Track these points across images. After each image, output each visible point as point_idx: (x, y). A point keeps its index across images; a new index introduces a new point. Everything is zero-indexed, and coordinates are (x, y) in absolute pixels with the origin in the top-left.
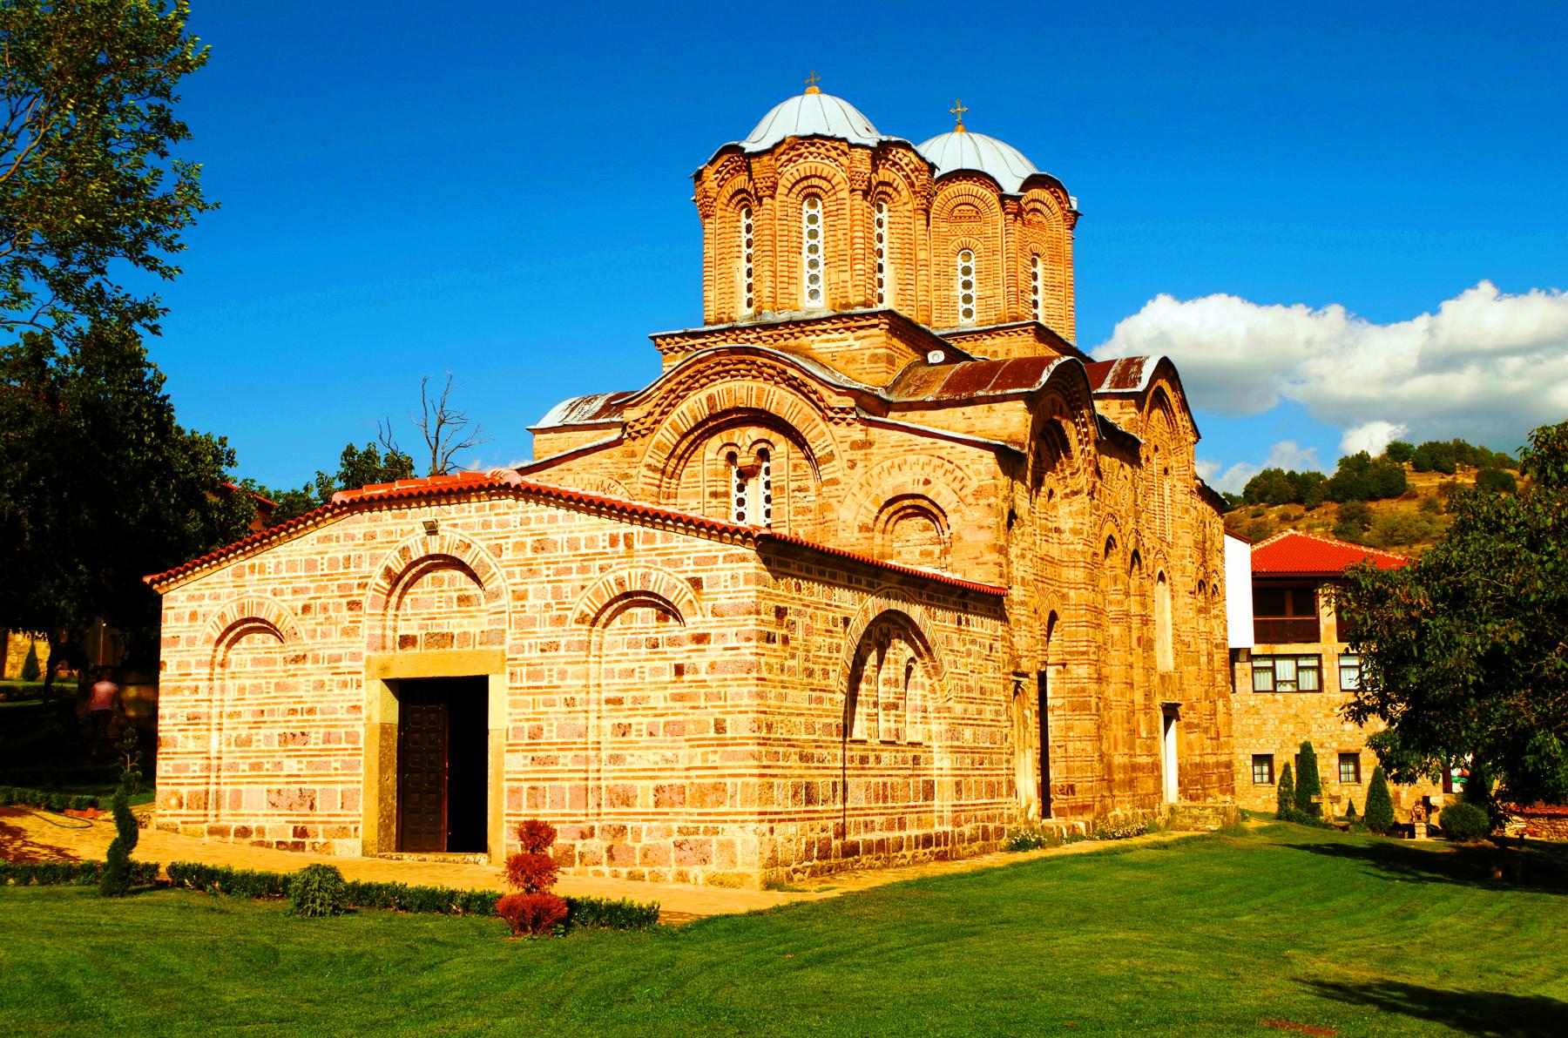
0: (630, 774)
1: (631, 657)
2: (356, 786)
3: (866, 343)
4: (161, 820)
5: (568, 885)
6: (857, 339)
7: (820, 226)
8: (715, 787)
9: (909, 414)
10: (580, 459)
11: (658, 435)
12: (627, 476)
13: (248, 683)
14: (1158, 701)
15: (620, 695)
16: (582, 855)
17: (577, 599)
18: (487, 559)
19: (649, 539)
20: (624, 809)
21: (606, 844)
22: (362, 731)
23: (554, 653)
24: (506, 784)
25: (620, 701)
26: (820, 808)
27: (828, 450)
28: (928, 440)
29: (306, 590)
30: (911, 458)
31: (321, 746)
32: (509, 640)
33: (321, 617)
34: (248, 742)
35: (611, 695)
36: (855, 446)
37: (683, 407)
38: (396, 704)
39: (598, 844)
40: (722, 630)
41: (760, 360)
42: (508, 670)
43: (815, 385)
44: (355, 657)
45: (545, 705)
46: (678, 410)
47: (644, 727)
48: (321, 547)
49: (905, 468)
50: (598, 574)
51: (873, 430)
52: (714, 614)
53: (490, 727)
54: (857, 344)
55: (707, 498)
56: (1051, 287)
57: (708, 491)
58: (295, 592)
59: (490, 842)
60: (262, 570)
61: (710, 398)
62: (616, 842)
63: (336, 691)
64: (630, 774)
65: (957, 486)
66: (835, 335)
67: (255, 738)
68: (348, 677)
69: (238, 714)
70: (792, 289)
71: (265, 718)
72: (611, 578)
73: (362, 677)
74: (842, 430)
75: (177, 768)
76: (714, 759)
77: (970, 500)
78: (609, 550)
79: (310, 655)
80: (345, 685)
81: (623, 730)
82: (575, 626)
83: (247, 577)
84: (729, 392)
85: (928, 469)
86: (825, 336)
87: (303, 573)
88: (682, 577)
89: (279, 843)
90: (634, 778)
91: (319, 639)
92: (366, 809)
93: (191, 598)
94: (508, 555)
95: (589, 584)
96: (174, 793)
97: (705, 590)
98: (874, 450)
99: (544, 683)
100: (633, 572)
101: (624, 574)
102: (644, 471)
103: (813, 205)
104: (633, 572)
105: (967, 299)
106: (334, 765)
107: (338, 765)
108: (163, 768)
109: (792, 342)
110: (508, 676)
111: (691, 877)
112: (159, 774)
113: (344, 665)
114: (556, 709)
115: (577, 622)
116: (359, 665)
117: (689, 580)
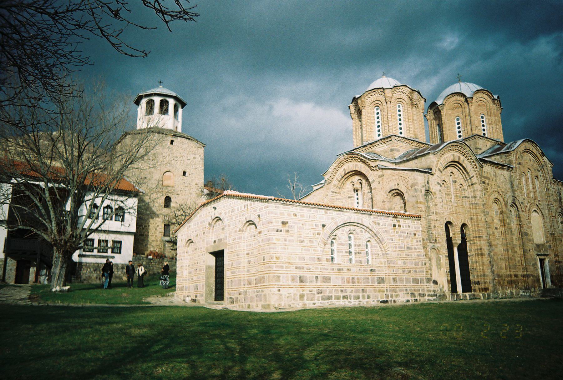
11: (333, 183)
12: (327, 195)
19: (251, 205)
26: (308, 284)
28: (398, 171)
30: (394, 178)
36: (380, 177)
37: (338, 173)
38: (214, 258)
41: (354, 156)
43: (367, 161)
49: (392, 181)
51: (384, 171)
53: (225, 263)
56: (490, 124)
61: (344, 169)
65: (406, 184)
66: (381, 145)
70: (372, 135)
74: (376, 173)
76: (263, 269)
77: (410, 188)
85: (398, 180)
86: (378, 146)
98: (384, 177)
103: (377, 109)
105: (459, 132)
109: (371, 150)
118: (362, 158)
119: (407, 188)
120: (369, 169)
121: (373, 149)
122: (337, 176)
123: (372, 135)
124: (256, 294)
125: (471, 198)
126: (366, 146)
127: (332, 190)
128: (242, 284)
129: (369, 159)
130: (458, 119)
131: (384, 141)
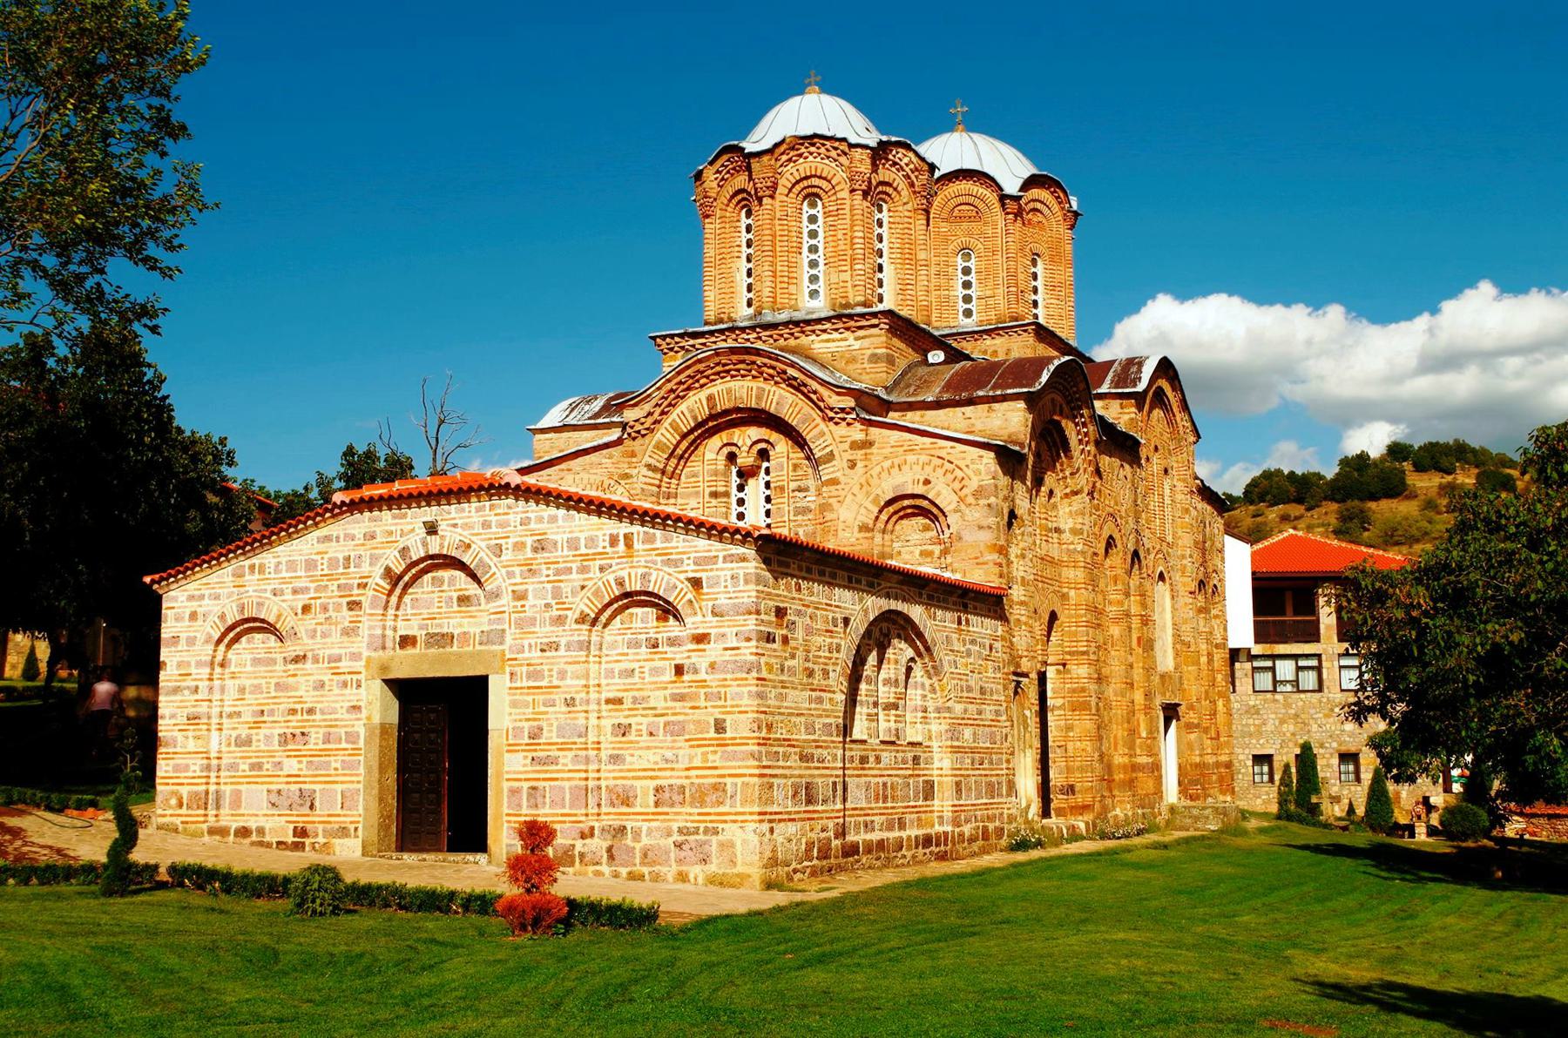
6: (857, 339)
9: (909, 414)
11: (658, 436)
12: (627, 476)
15: (620, 695)
16: (582, 855)
18: (486, 559)
20: (624, 809)
21: (605, 845)
22: (362, 731)
23: (554, 653)
25: (620, 701)
26: (820, 808)
29: (305, 590)
30: (911, 458)
32: (509, 640)
33: (321, 617)
35: (611, 695)
36: (855, 446)
37: (683, 407)
40: (722, 630)
41: (759, 360)
42: (508, 670)
43: (815, 385)
44: (355, 657)
46: (678, 411)
47: (644, 727)
50: (598, 574)
51: (873, 430)
52: (714, 614)
54: (857, 345)
55: (707, 498)
56: (1051, 287)
57: (707, 491)
58: (295, 592)
60: (262, 569)
61: (710, 398)
63: (336, 691)
65: (957, 485)
66: (835, 335)
68: (348, 677)
69: (239, 714)
70: (793, 289)
71: (265, 718)
72: (611, 578)
73: (362, 677)
74: (842, 430)
75: (177, 768)
77: (971, 500)
78: (609, 550)
79: (309, 655)
80: (345, 685)
81: (623, 730)
84: (729, 391)
85: (928, 469)
86: (825, 336)
87: (303, 573)
88: (682, 577)
89: (279, 843)
90: (634, 778)
92: (366, 809)
93: (191, 598)
94: (507, 555)
96: (174, 793)
97: (705, 590)
98: (874, 450)
99: (544, 683)
100: (633, 572)
102: (644, 471)
103: (813, 205)
104: (633, 572)
105: (967, 299)
106: (334, 765)
108: (163, 768)
109: (792, 342)
110: (508, 677)
113: (345, 665)
114: (556, 709)
115: (577, 622)
117: (689, 580)
118: (791, 372)
119: (962, 499)
120: (816, 414)
121: (804, 340)
122: (674, 415)
123: (793, 289)
124: (677, 837)
125: (1067, 536)
126: (774, 326)
127: (647, 460)
128: (592, 801)
129: (824, 383)
130: (967, 257)
131: (840, 325)
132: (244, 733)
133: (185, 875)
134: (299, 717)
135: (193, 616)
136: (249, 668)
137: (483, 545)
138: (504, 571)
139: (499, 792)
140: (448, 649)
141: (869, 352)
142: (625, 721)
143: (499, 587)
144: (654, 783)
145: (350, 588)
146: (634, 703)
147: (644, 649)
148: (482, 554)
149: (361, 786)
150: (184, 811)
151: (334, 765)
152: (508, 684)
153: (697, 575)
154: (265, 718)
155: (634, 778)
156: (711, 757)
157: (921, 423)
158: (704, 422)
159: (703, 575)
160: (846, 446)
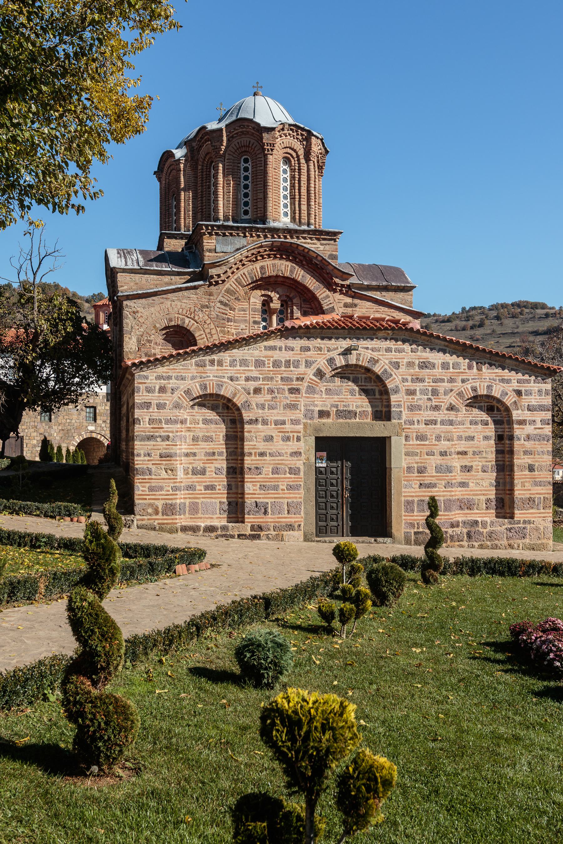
0: (472, 493)
1: (472, 430)
2: (299, 500)
3: (327, 247)
4: (140, 523)
5: (448, 552)
6: (321, 244)
7: (249, 165)
8: (530, 499)
9: (384, 293)
10: (176, 294)
11: (227, 285)
13: (201, 434)
14: (171, 434)
15: (465, 450)
16: (452, 537)
17: (447, 397)
18: (389, 370)
20: (469, 512)
21: (465, 531)
22: (302, 468)
23: (434, 426)
24: (403, 499)
25: (465, 453)
27: (331, 306)
29: (256, 379)
31: (271, 476)
32: (404, 417)
33: (269, 397)
34: (203, 472)
35: (460, 450)
39: (462, 530)
40: (533, 418)
42: (404, 434)
44: (295, 422)
45: (427, 455)
46: (242, 272)
47: (480, 468)
48: (269, 353)
50: (460, 384)
52: (529, 410)
54: (322, 248)
55: (251, 324)
57: (252, 320)
58: (247, 379)
59: (394, 531)
60: (220, 363)
61: (262, 268)
62: (473, 530)
63: (281, 442)
64: (472, 493)
67: (208, 469)
68: (291, 435)
69: (194, 454)
71: (216, 457)
72: (469, 387)
73: (301, 435)
75: (151, 489)
78: (467, 371)
79: (260, 419)
80: (288, 439)
81: (467, 469)
82: (446, 412)
83: (208, 367)
84: (274, 265)
87: (253, 368)
88: (511, 389)
89: (239, 536)
90: (473, 495)
91: (266, 410)
92: (306, 514)
93: (159, 378)
94: (403, 369)
95: (455, 389)
96: (151, 505)
97: (524, 397)
99: (427, 443)
100: (482, 384)
101: (477, 384)
102: (218, 305)
104: (482, 384)
106: (281, 487)
107: (220, 487)
108: (140, 488)
110: (403, 438)
111: (516, 546)
112: (136, 492)
113: (288, 427)
114: (435, 457)
115: (447, 409)
116: (300, 427)
117: (514, 390)
127: (220, 298)
132: (199, 465)
133: (473, 567)
134: (253, 458)
135: (162, 390)
136: (201, 425)
137: (387, 362)
138: (400, 377)
139: (399, 503)
140: (353, 420)
141: (329, 253)
142: (468, 464)
143: (397, 387)
144: (486, 497)
145: (291, 380)
146: (474, 455)
147: (480, 425)
148: (386, 367)
149: (302, 500)
150: (160, 516)
151: (281, 487)
152: (404, 442)
153: (520, 389)
154: (216, 457)
155: (473, 495)
156: (526, 484)
157: (391, 300)
158: (257, 281)
159: (523, 389)
160: (342, 305)
